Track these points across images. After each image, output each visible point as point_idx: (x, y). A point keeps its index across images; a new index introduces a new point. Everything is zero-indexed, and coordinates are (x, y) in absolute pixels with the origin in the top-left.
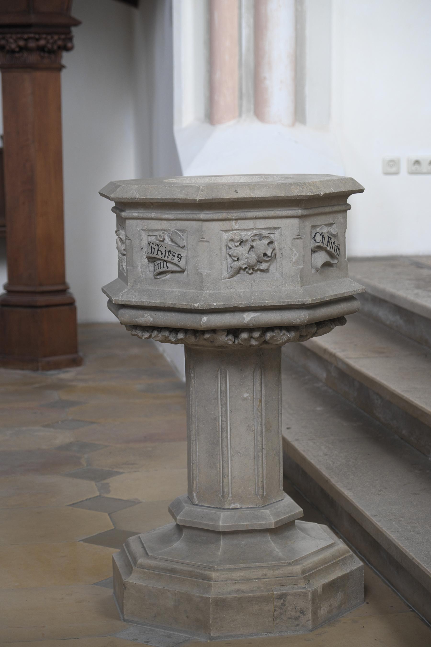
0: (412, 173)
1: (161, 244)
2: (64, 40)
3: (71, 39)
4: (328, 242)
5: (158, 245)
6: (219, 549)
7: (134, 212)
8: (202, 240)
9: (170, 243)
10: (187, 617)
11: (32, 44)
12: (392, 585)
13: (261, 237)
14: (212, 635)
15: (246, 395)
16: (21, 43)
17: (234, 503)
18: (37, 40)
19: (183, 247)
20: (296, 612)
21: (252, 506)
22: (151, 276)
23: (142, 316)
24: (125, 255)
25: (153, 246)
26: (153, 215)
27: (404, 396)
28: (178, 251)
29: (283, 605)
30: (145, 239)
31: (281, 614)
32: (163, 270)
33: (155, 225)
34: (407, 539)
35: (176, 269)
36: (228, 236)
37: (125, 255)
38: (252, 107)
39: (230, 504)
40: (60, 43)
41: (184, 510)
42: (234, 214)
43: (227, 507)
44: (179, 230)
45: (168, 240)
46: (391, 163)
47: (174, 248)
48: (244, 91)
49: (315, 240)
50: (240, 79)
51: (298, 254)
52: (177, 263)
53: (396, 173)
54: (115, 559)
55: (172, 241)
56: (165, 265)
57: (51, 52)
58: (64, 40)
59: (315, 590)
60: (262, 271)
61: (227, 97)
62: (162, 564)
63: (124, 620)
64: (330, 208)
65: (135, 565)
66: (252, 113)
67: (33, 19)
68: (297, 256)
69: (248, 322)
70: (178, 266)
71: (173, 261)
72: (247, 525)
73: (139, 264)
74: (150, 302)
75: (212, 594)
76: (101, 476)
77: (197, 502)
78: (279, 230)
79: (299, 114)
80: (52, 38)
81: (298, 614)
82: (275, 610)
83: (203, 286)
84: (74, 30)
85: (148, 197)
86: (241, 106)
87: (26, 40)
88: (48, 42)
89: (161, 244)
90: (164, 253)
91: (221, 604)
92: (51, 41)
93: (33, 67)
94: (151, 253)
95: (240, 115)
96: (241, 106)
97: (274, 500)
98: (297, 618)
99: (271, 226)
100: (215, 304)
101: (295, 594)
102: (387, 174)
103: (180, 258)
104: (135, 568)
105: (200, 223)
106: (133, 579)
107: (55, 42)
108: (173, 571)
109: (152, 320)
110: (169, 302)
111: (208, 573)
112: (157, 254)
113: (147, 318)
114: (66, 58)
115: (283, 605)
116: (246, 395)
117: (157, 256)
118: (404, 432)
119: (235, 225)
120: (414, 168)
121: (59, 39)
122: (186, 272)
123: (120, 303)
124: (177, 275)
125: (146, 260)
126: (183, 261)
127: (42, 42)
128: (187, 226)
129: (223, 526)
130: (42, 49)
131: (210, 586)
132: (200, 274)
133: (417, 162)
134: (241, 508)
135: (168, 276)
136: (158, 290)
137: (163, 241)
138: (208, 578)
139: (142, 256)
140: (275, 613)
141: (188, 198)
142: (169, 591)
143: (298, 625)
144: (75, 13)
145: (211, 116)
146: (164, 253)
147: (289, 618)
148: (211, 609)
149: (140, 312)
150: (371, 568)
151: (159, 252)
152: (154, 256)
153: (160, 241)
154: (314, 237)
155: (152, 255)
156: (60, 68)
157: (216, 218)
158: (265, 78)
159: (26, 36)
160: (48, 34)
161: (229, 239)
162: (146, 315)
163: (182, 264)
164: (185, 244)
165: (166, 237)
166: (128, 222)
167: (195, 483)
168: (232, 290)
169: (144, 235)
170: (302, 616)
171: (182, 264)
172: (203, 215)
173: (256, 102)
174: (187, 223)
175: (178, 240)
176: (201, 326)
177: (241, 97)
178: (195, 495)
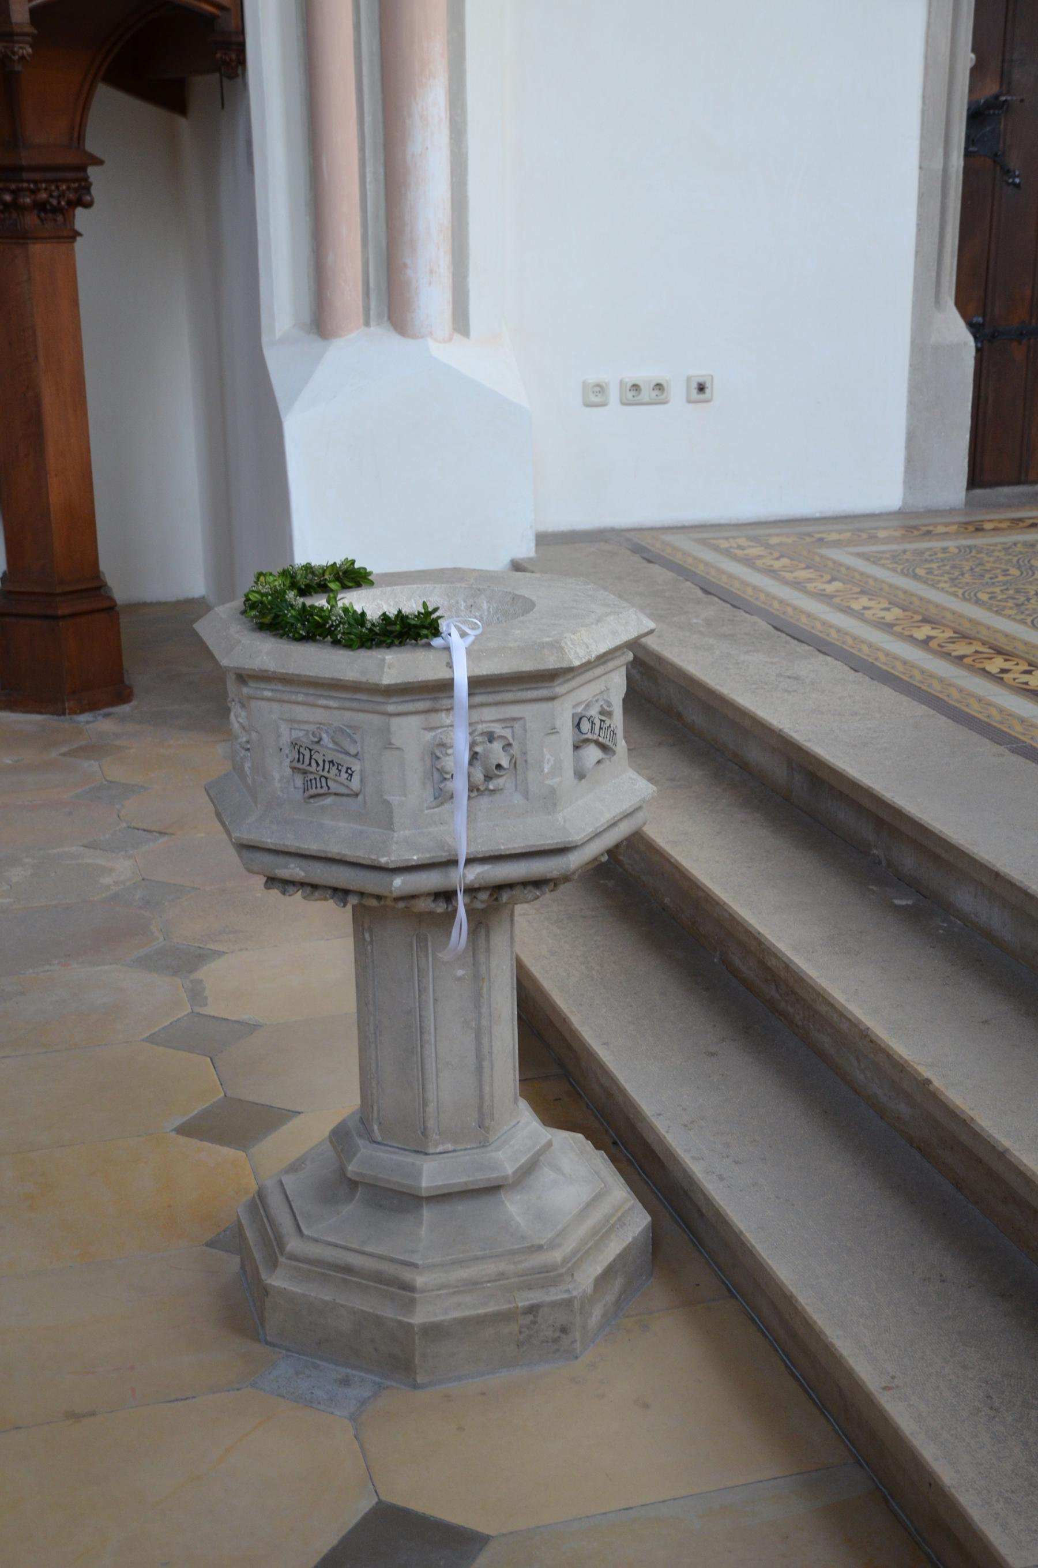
0: (625, 403)
1: (316, 747)
2: (76, 190)
3: (87, 188)
4: (601, 728)
5: (311, 750)
6: (421, 1223)
7: (265, 689)
9: (331, 745)
10: (376, 1349)
12: (690, 1230)
14: (419, 1381)
15: (460, 973)
17: (443, 1144)
19: (356, 756)
20: (554, 1331)
21: (474, 1146)
22: (299, 795)
23: (286, 867)
24: (248, 750)
25: (302, 750)
27: (672, 857)
28: (348, 761)
29: (534, 1322)
31: (530, 1336)
32: (320, 791)
33: (302, 713)
34: (721, 1178)
35: (343, 790)
36: (434, 738)
37: (248, 750)
38: (386, 309)
39: (436, 1146)
40: (71, 196)
41: (359, 1155)
43: (431, 1151)
44: (348, 727)
45: (326, 740)
46: (598, 389)
47: (339, 757)
48: (372, 285)
49: (579, 729)
51: (552, 759)
52: (346, 782)
53: (604, 404)
54: (243, 1222)
56: (324, 784)
57: (57, 210)
58: (76, 190)
59: (584, 1291)
60: (493, 792)
62: (328, 1254)
63: (267, 1343)
64: (602, 667)
65: (282, 1253)
66: (386, 319)
68: (552, 762)
69: (471, 881)
70: (347, 787)
71: (338, 779)
72: (466, 1183)
73: (277, 776)
74: (299, 848)
75: (419, 1318)
76: (184, 961)
77: (379, 1139)
78: (521, 722)
80: (57, 187)
81: (558, 1334)
82: (521, 1332)
83: (392, 824)
84: (92, 171)
85: (290, 672)
86: (367, 309)
87: (13, 192)
88: (51, 196)
89: (316, 747)
90: (321, 763)
91: (434, 1332)
92: (55, 194)
94: (299, 761)
95: (367, 323)
97: (506, 1128)
98: (555, 1340)
99: (507, 716)
100: (415, 858)
101: (553, 1304)
102: (588, 405)
103: (351, 775)
104: (282, 1260)
105: (384, 718)
106: (277, 1280)
107: (62, 195)
108: (348, 1269)
109: (302, 874)
110: (335, 849)
111: (407, 1275)
112: (310, 765)
113: (294, 870)
114: (81, 218)
115: (534, 1322)
116: (460, 973)
117: (309, 768)
118: (667, 900)
120: (630, 395)
121: (69, 188)
122: (360, 797)
123: (245, 842)
124: (345, 799)
125: (289, 771)
126: (356, 778)
129: (427, 1188)
131: (412, 1302)
132: (387, 803)
133: (636, 387)
134: (454, 1151)
135: (329, 800)
136: (311, 822)
137: (318, 742)
138: (409, 1287)
139: (281, 762)
140: (521, 1337)
141: (364, 679)
142: (342, 1306)
143: (558, 1350)
144: (91, 146)
145: (320, 322)
146: (321, 763)
147: (542, 1342)
148: (417, 1341)
149: (280, 860)
150: (647, 1183)
151: (313, 762)
152: (304, 767)
153: (313, 742)
154: (579, 724)
155: (299, 765)
157: (414, 710)
158: (405, 265)
159: (13, 186)
160: (52, 181)
161: (437, 743)
162: (292, 866)
163: (355, 784)
164: (359, 749)
165: (324, 736)
167: (375, 1108)
168: (442, 828)
169: (284, 729)
170: (563, 1336)
171: (355, 784)
174: (361, 715)
175: (347, 744)
176: (391, 892)
178: (376, 1127)
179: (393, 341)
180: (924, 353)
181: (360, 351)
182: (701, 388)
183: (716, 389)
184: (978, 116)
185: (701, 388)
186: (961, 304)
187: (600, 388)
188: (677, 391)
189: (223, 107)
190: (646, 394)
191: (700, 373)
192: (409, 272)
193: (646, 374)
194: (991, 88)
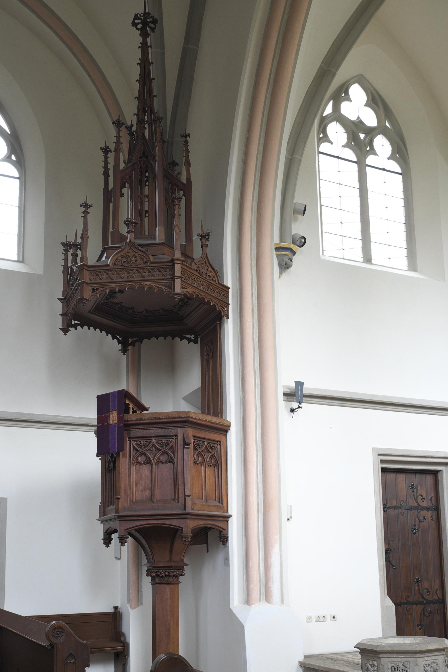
8: (416, 665)
11: (172, 574)
13: (434, 663)
16: (167, 574)
18: (173, 572)
26: (395, 656)
30: (390, 665)
33: (394, 660)
42: (426, 655)
50: (260, 587)
55: (403, 665)
61: (255, 594)
67: (173, 564)
79: (282, 602)
86: (260, 598)
87: (169, 572)
93: (171, 583)
95: (260, 601)
96: (260, 598)
114: (181, 578)
119: (426, 659)
127: (175, 573)
128: (410, 660)
130: (174, 576)
145: (248, 601)
156: (179, 583)
166: (382, 659)
172: (417, 656)
173: (267, 596)
177: (260, 594)
179: (268, 605)
180: (384, 608)
181: (259, 608)
182: (334, 617)
183: (337, 617)
184: (387, 552)
185: (334, 617)
186: (388, 594)
187: (310, 617)
188: (329, 618)
189: (208, 552)
190: (321, 619)
191: (333, 614)
192: (272, 588)
193: (321, 614)
194: (387, 547)
